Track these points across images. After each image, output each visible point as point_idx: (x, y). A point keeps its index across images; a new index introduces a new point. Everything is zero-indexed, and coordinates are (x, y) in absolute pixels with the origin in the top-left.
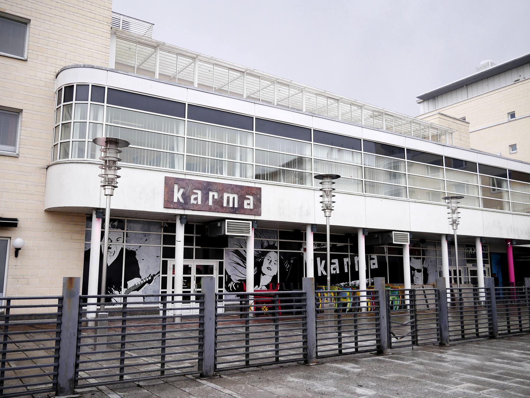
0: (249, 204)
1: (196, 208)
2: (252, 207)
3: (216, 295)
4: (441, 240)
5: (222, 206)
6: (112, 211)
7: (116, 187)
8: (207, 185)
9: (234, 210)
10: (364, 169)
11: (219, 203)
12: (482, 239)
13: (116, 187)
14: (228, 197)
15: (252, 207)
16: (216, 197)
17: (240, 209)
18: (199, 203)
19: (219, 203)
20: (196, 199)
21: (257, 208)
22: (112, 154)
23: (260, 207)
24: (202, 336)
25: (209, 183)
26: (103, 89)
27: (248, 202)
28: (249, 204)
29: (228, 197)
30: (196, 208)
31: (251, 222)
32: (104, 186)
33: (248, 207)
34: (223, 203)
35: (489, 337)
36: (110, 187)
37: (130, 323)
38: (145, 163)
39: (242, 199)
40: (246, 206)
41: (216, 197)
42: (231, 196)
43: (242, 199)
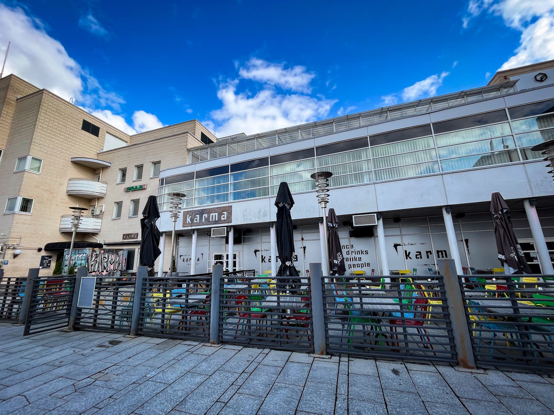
0: (224, 217)
1: (196, 225)
2: (226, 219)
3: (460, 278)
4: (524, 209)
5: (209, 221)
6: (176, 231)
7: (328, 202)
8: (202, 212)
9: (216, 222)
10: (440, 162)
11: (207, 219)
12: (533, 201)
13: (328, 202)
14: (212, 215)
15: (226, 219)
16: (206, 217)
17: (219, 221)
18: (198, 222)
19: (207, 219)
20: (196, 220)
21: (229, 219)
22: (176, 200)
23: (231, 217)
24: (448, 320)
25: (203, 210)
26: (429, 126)
27: (224, 216)
28: (224, 217)
29: (212, 215)
30: (196, 225)
31: (376, 214)
32: (320, 202)
33: (224, 219)
34: (209, 219)
35: (12, 294)
36: (323, 203)
37: (526, 314)
38: (341, 185)
39: (220, 214)
40: (222, 219)
41: (206, 217)
42: (214, 214)
43: (220, 214)
